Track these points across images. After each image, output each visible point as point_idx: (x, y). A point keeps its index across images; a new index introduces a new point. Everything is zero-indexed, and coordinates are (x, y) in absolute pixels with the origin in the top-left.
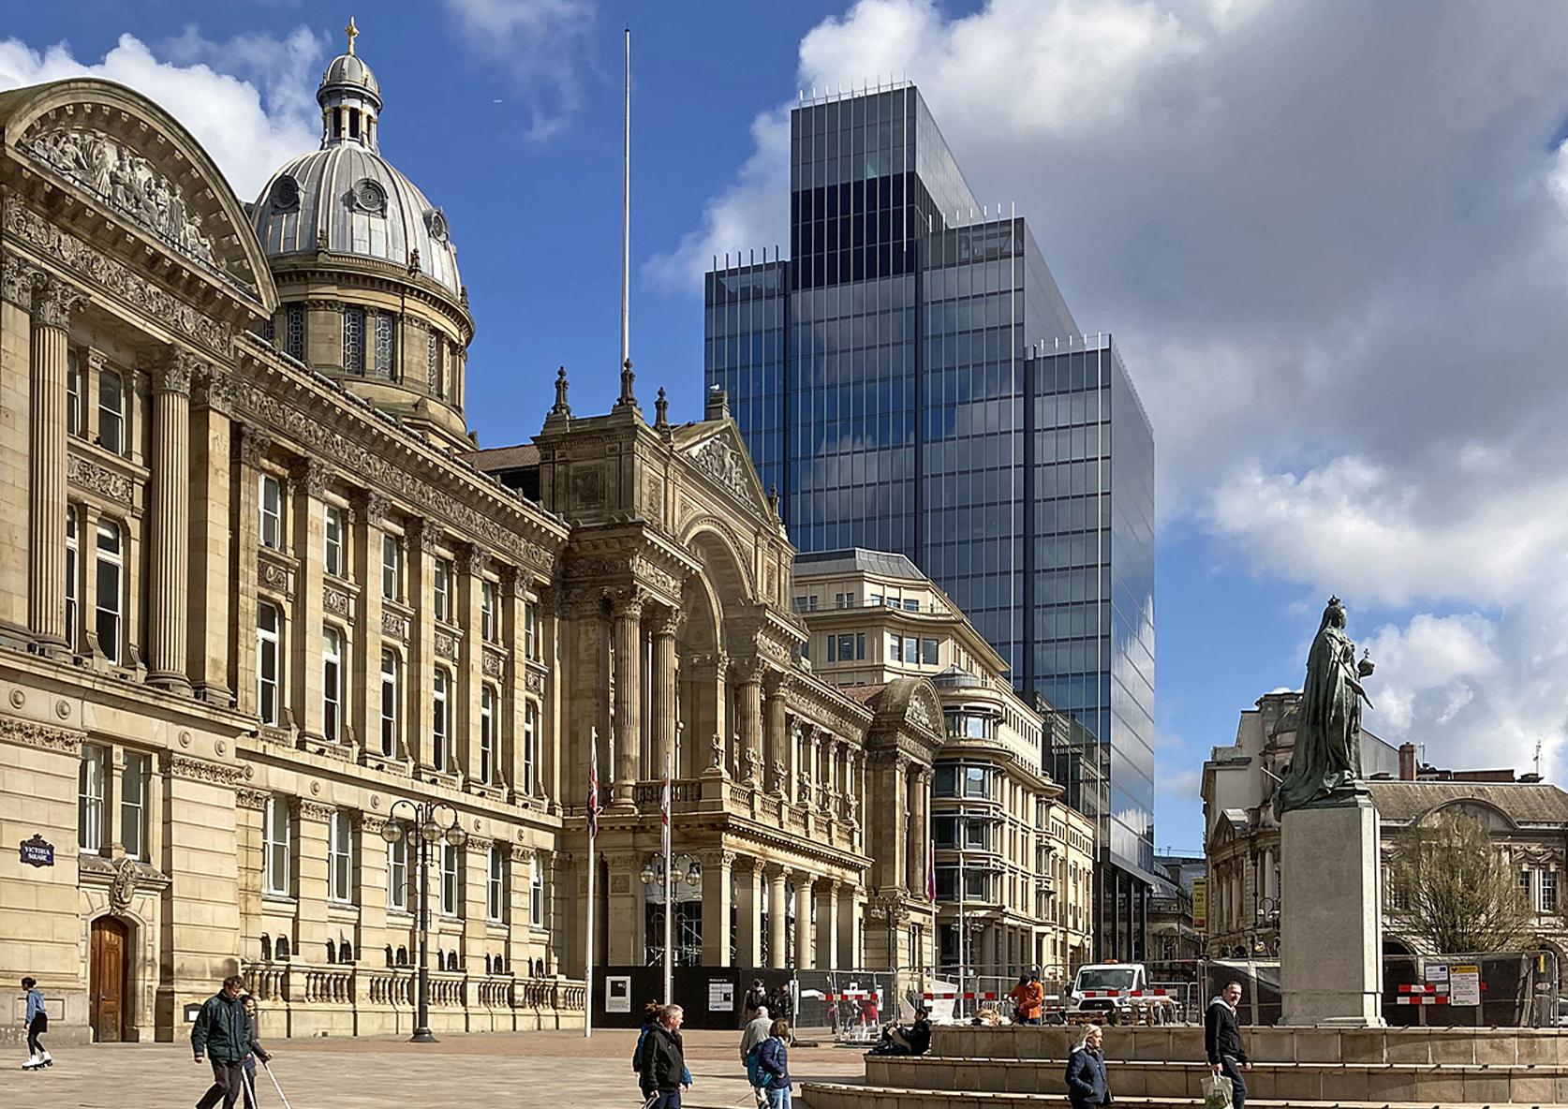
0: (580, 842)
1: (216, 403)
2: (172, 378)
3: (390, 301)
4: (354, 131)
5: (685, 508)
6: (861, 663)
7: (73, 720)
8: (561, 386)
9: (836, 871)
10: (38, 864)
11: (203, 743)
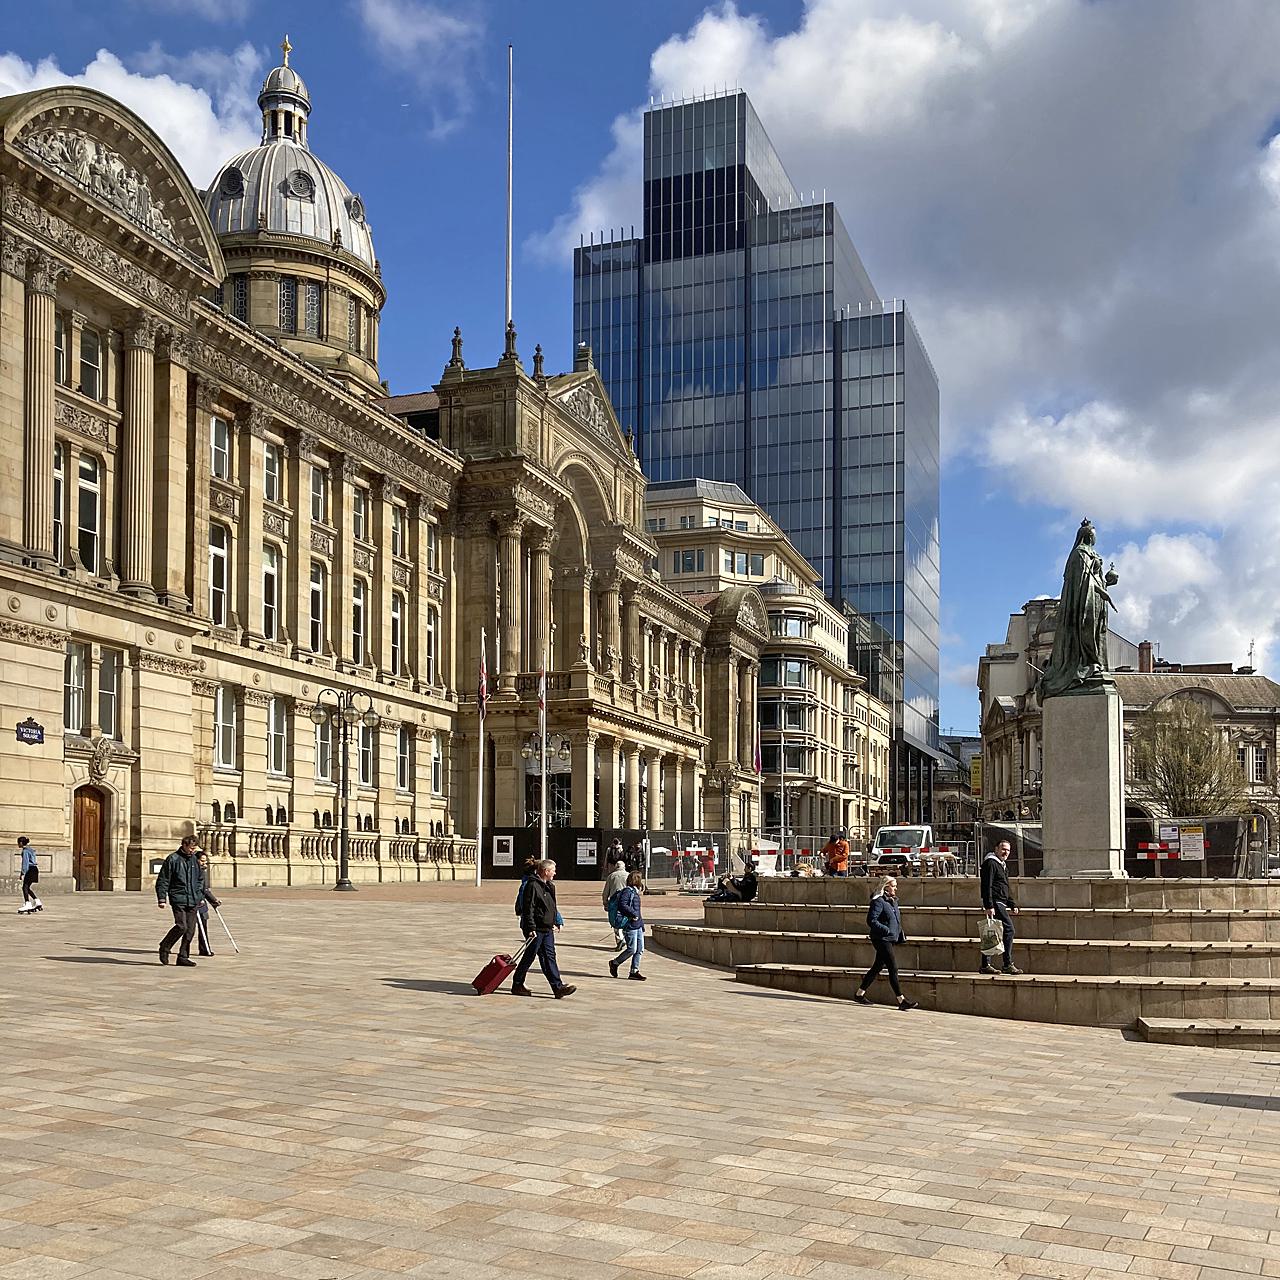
1: (176, 357)
3: (317, 272)
6: (701, 574)
7: (59, 622)
8: (456, 343)
9: (681, 748)
10: (30, 742)
11: (165, 642)
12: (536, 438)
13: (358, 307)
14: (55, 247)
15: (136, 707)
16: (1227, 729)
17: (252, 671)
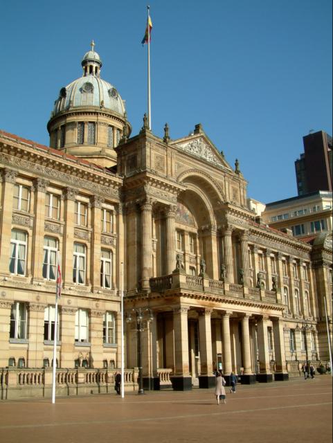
3: (93, 118)
4: (91, 71)
5: (179, 166)
6: (304, 235)
9: (264, 310)
13: (113, 130)
15: (28, 326)
17: (95, 303)
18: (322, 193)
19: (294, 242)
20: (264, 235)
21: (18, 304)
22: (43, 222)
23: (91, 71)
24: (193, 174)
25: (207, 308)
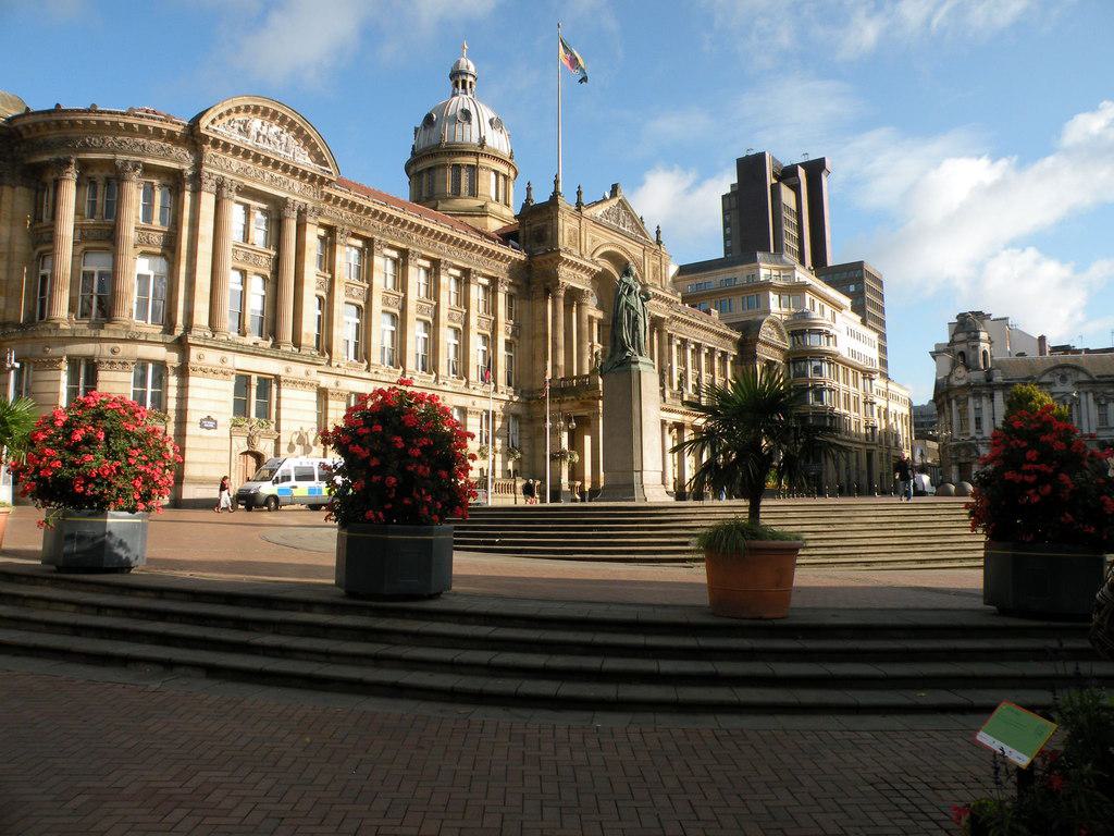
0: (50, 375)
2: (287, 212)
3: (471, 160)
4: (464, 87)
7: (229, 364)
8: (529, 189)
11: (298, 370)
12: (577, 238)
14: (236, 174)
15: (278, 408)
16: (1091, 391)
18: (759, 255)
19: (721, 330)
20: (686, 322)
21: (150, 366)
22: (447, 311)
23: (464, 87)
24: (608, 249)
25: (687, 424)
